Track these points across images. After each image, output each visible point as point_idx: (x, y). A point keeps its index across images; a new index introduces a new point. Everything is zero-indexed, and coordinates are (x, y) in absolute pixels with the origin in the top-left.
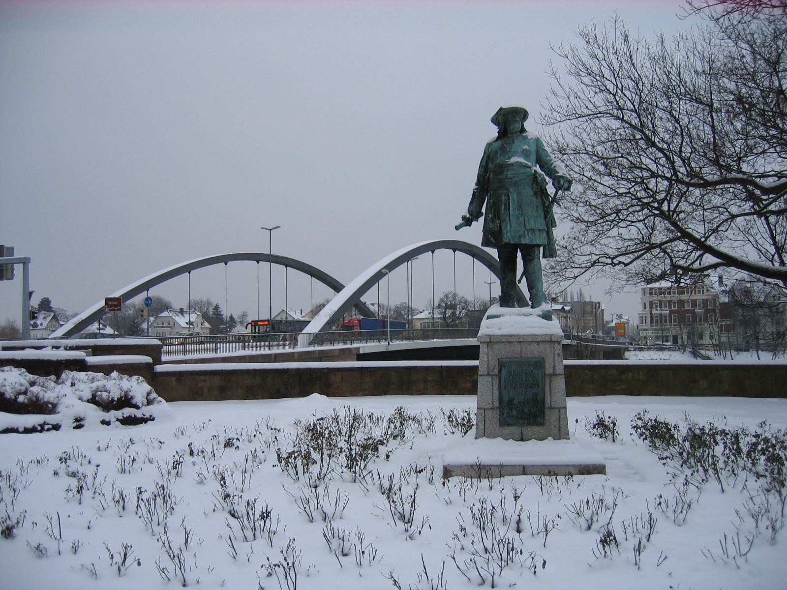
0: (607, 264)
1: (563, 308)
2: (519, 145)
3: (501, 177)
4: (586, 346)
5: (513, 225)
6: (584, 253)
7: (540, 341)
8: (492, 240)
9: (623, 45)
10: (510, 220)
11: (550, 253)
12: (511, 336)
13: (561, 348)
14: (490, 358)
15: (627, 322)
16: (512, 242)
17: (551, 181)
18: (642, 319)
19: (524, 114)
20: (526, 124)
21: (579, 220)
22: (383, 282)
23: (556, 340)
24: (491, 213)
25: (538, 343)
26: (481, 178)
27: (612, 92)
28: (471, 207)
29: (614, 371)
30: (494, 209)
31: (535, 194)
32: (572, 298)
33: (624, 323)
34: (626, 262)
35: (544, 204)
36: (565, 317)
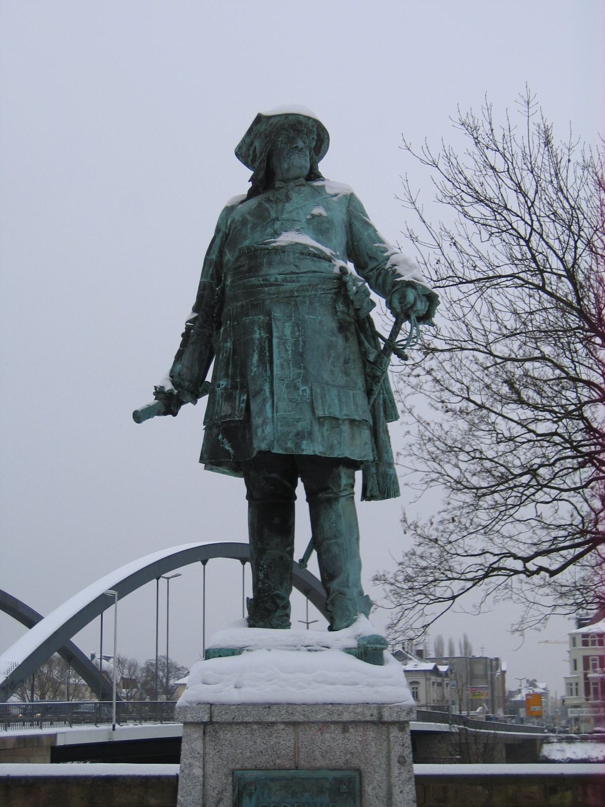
0: (516, 572)
1: (435, 667)
2: (300, 204)
3: (254, 281)
4: (476, 736)
5: (282, 405)
6: (470, 552)
7: (351, 722)
8: (227, 447)
9: (541, 151)
10: (272, 393)
11: (382, 487)
12: (269, 706)
13: (408, 742)
14: (210, 767)
15: (545, 694)
16: (277, 450)
17: (383, 301)
18: (571, 687)
19: (318, 135)
20: (323, 167)
21: (459, 485)
22: (108, 613)
23: (394, 717)
24: (227, 376)
25: (345, 726)
26: (206, 292)
27: (523, 233)
28: (179, 366)
29: (535, 788)
30: (235, 367)
31: (342, 328)
32: (451, 651)
33: (539, 696)
34: (554, 567)
35: (364, 355)
36: (440, 684)
